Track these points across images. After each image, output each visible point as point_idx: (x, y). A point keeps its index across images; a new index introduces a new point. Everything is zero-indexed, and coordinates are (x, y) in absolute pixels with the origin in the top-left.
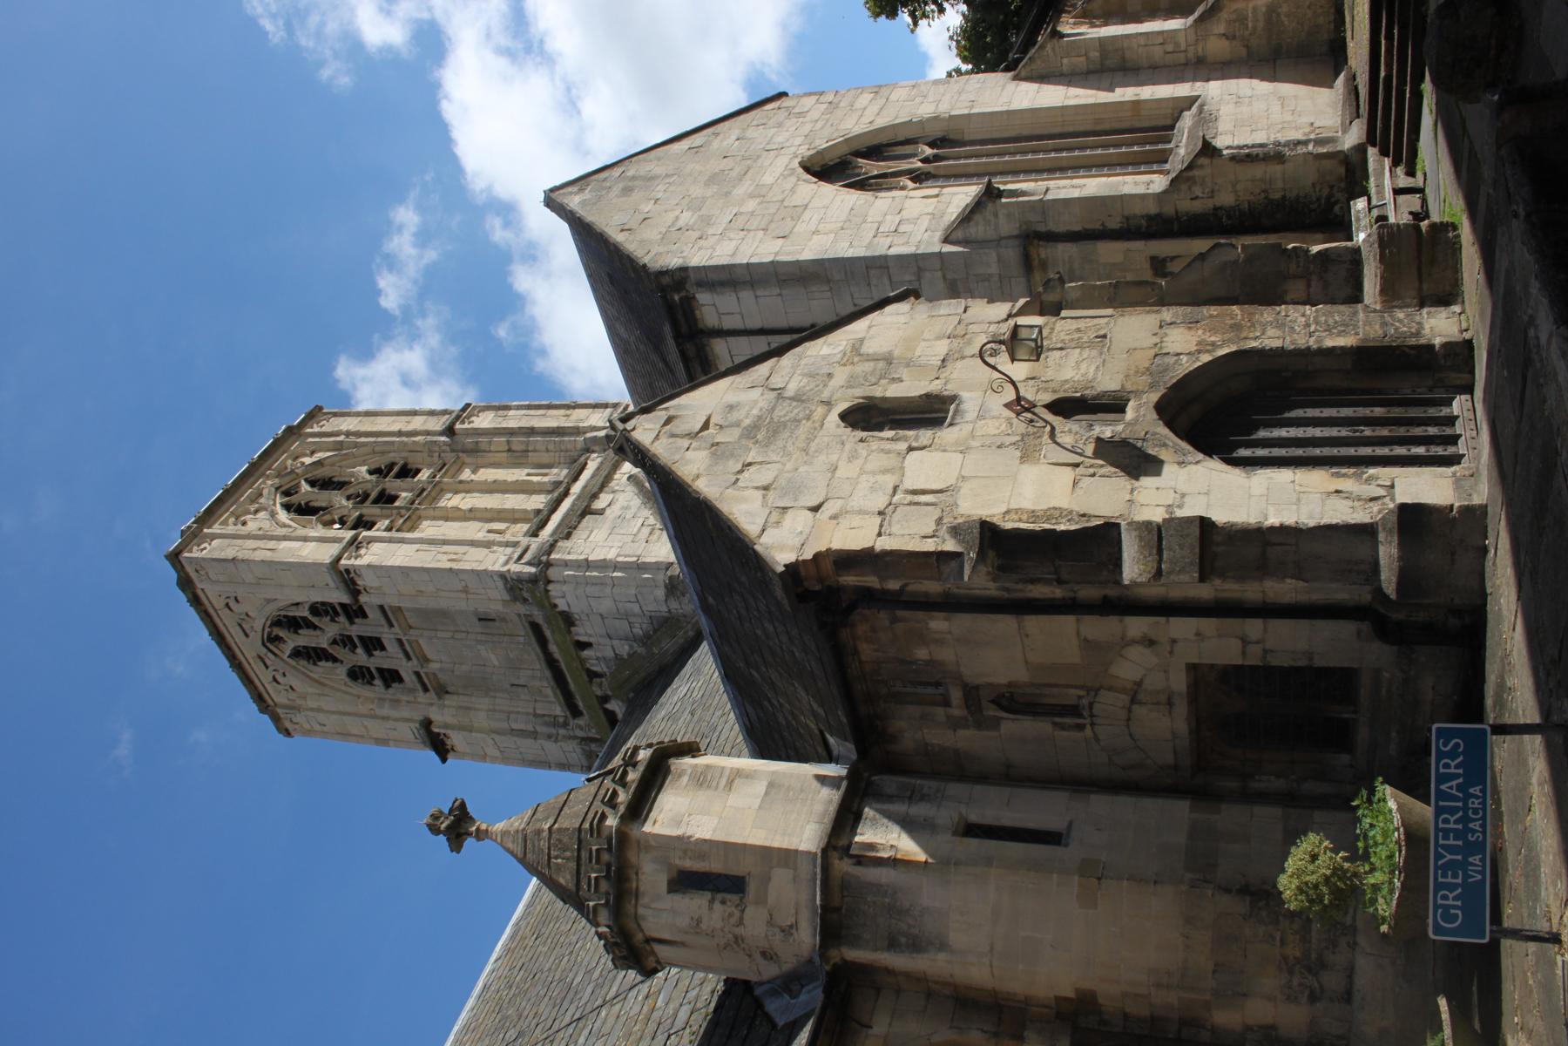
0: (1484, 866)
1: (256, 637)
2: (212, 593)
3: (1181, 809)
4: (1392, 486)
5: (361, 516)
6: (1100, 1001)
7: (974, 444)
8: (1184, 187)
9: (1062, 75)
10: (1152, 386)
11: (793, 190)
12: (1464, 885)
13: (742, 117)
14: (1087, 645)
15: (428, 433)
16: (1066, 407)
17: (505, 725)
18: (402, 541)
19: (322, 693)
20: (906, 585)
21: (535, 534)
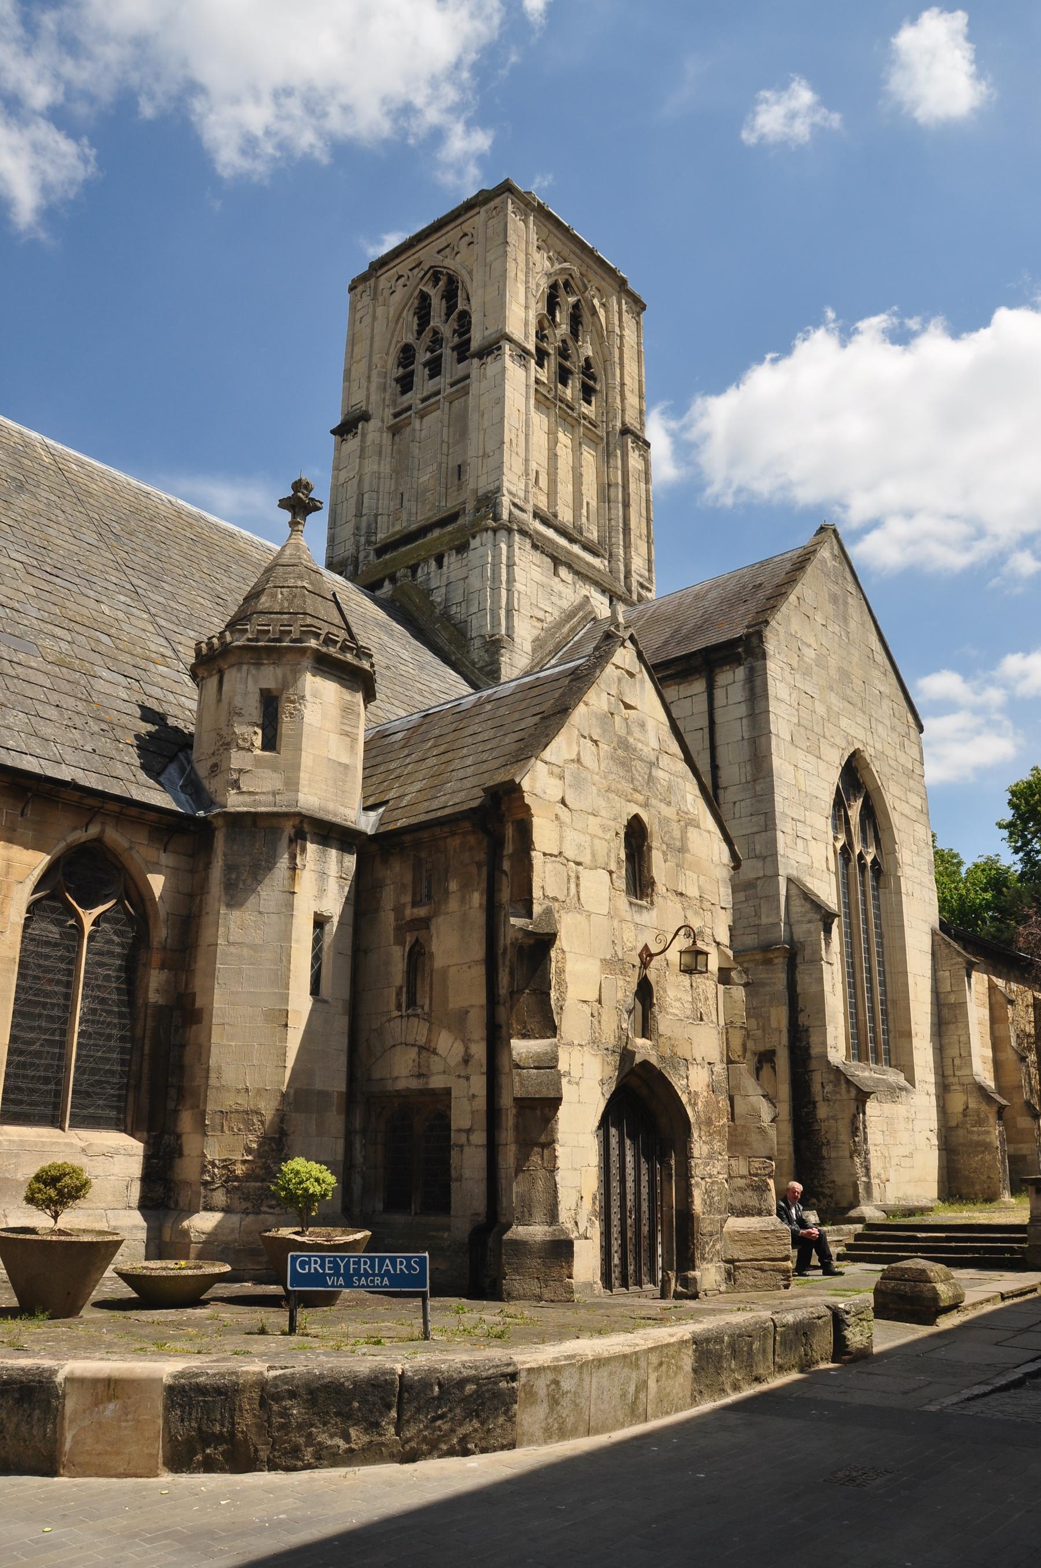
0: (337, 1287)
1: (438, 260)
2: (477, 220)
3: (340, 1085)
4: (586, 1238)
5: (548, 355)
6: (194, 1027)
7: (616, 923)
8: (832, 1077)
10: (662, 1058)
11: (833, 745)
12: (325, 1275)
13: (901, 694)
14: (463, 1014)
15: (623, 411)
16: (645, 991)
17: (366, 487)
18: (527, 398)
19: (391, 321)
20: (507, 875)
21: (536, 515)
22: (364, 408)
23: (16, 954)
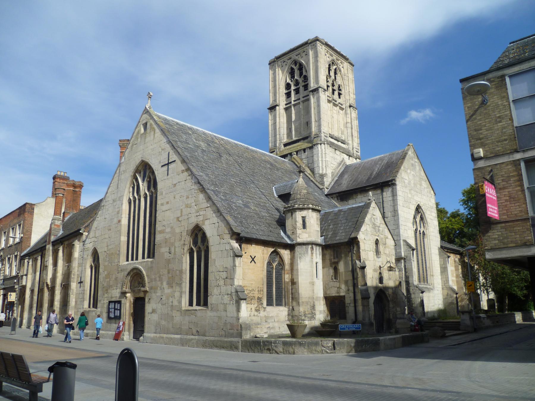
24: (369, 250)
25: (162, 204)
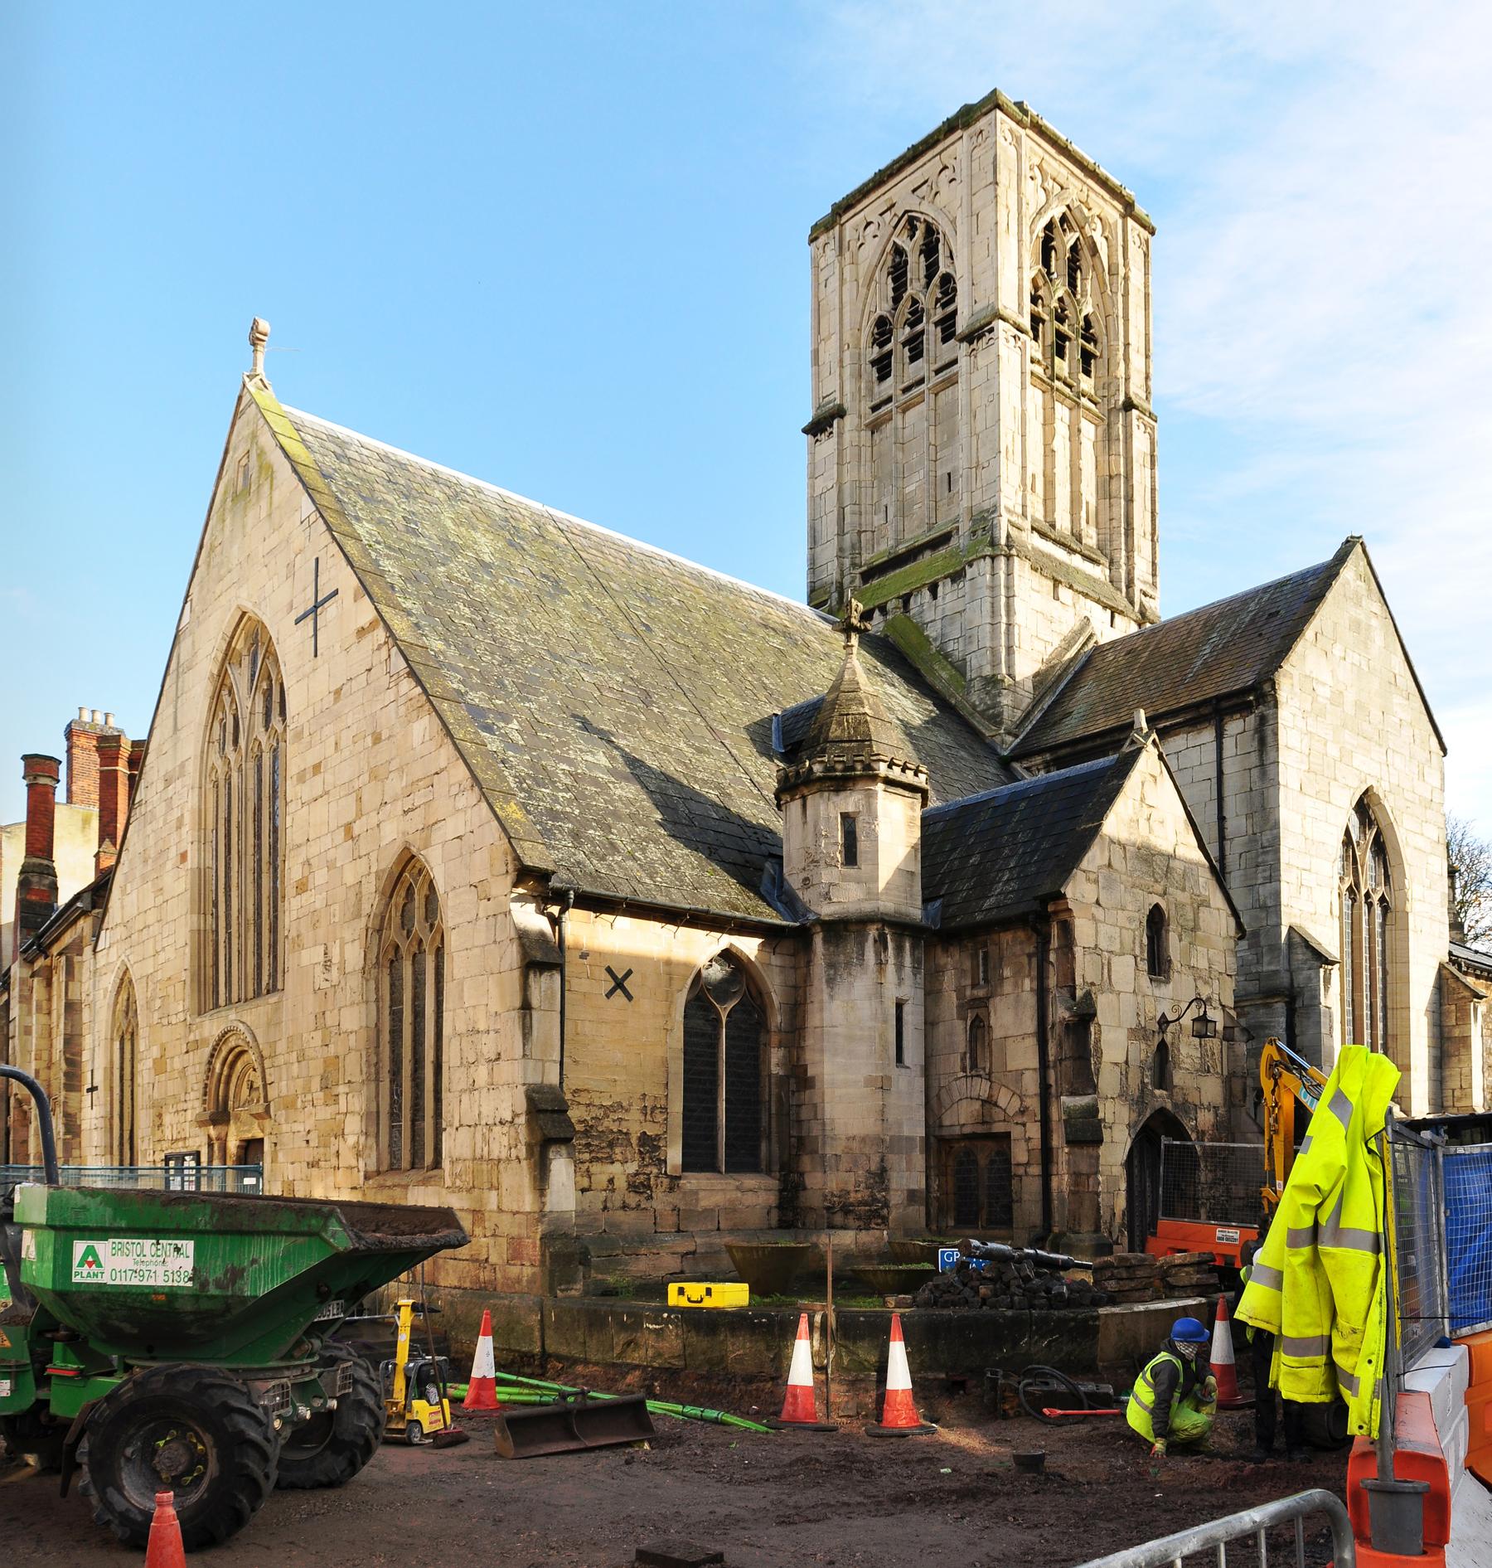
1: (912, 203)
2: (959, 146)
5: (1043, 321)
9: (1441, 1005)
15: (1127, 379)
17: (847, 502)
22: (838, 402)
23: (681, 1045)
24: (1116, 948)
25: (301, 778)
